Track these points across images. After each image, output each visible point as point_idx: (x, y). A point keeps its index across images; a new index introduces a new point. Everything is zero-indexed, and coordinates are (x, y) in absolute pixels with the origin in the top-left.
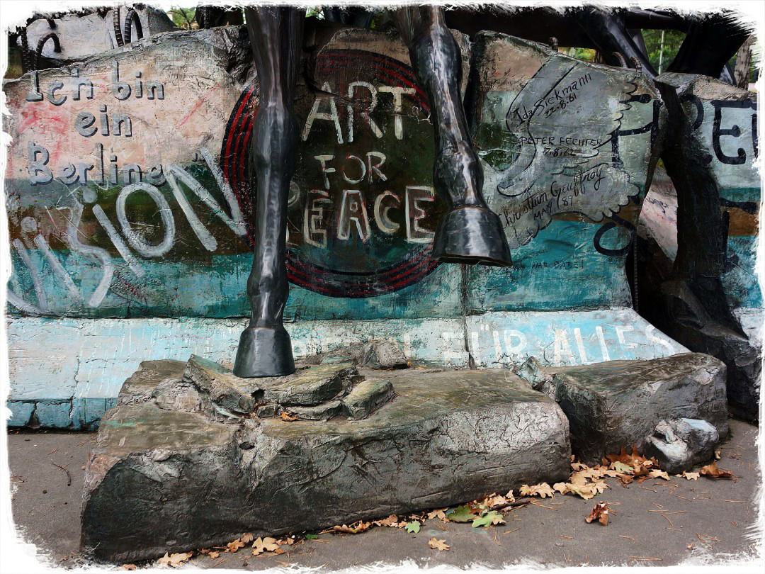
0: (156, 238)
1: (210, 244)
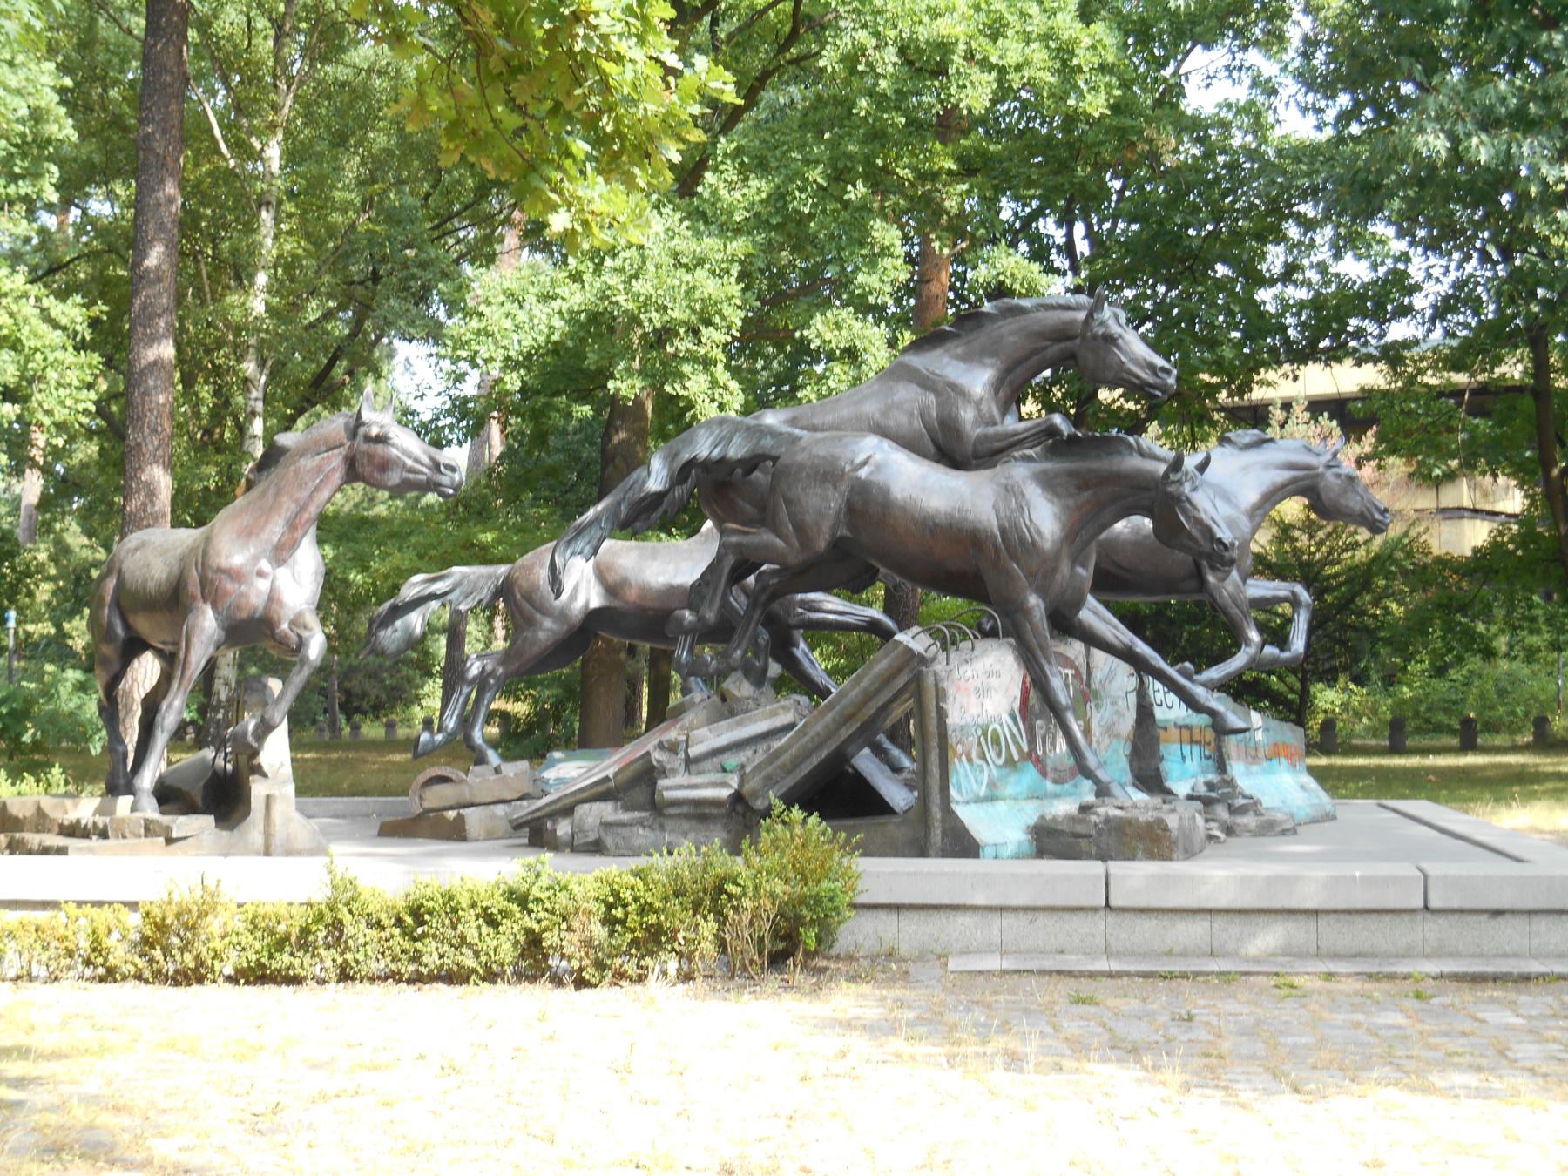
0: (999, 755)
1: (1016, 757)
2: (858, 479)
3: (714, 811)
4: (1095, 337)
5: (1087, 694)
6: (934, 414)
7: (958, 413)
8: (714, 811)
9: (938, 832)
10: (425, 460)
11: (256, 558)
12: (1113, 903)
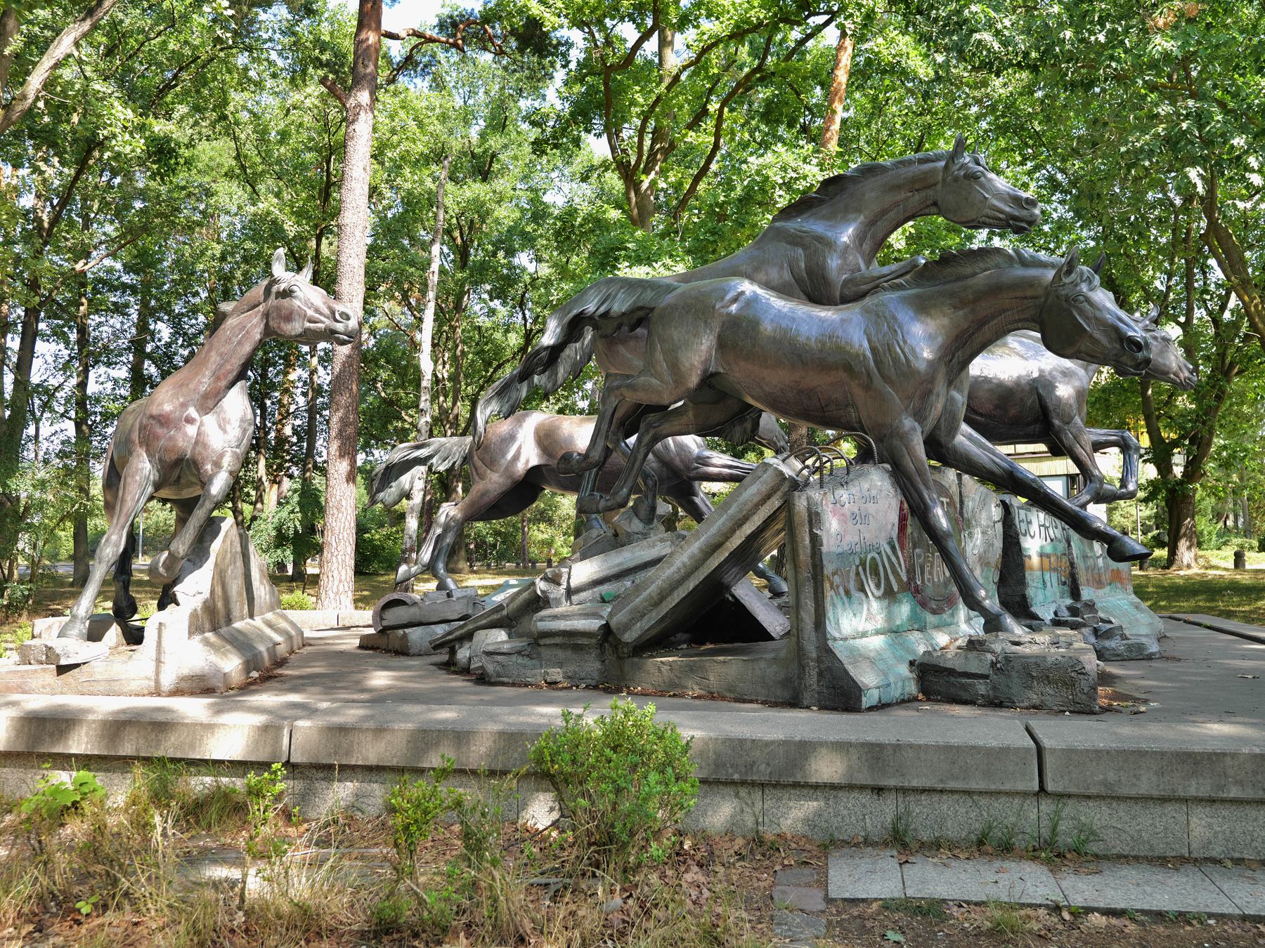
2: (729, 314)
3: (585, 641)
4: (956, 179)
5: (961, 520)
6: (803, 265)
7: (825, 261)
8: (585, 641)
9: (814, 673)
10: (327, 311)
11: (184, 406)
12: (1050, 787)
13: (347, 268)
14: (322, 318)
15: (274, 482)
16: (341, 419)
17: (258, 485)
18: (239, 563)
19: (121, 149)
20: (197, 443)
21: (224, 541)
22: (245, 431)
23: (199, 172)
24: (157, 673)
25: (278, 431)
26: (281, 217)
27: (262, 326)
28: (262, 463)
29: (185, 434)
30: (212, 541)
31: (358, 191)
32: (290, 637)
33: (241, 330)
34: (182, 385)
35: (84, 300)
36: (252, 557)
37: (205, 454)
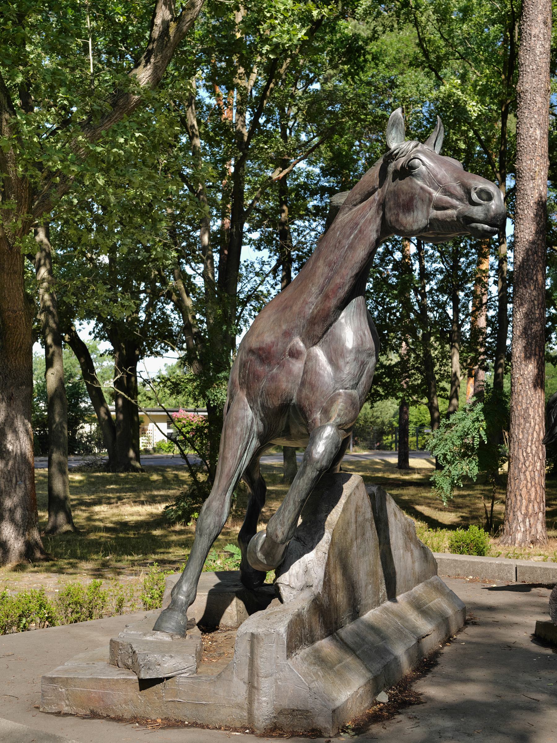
10: (459, 191)
11: (288, 335)
13: (529, 141)
14: (455, 202)
15: (470, 376)
16: (526, 315)
17: (453, 380)
18: (371, 533)
19: (279, 40)
20: (303, 384)
21: (344, 510)
22: (363, 364)
23: (387, 66)
24: (251, 702)
25: (472, 323)
26: (463, 97)
27: (378, 220)
28: (456, 358)
29: (290, 372)
30: (328, 511)
31: (539, 50)
32: (444, 621)
33: (353, 229)
34: (285, 308)
35: (285, 208)
36: (392, 520)
37: (313, 398)
